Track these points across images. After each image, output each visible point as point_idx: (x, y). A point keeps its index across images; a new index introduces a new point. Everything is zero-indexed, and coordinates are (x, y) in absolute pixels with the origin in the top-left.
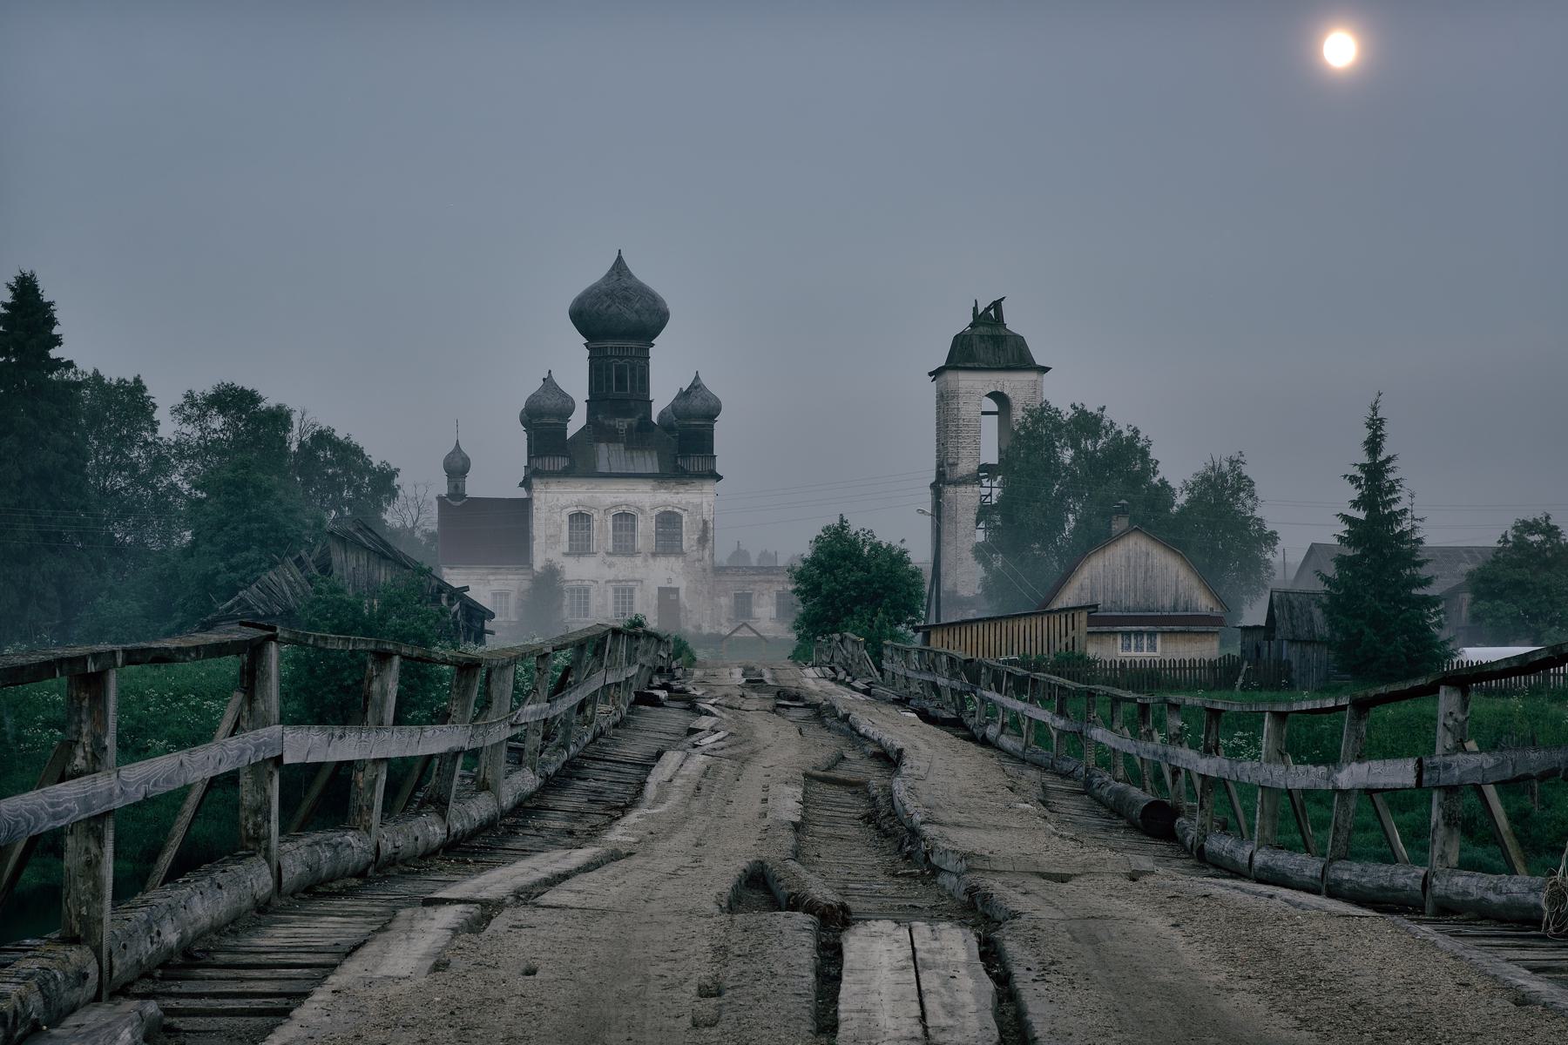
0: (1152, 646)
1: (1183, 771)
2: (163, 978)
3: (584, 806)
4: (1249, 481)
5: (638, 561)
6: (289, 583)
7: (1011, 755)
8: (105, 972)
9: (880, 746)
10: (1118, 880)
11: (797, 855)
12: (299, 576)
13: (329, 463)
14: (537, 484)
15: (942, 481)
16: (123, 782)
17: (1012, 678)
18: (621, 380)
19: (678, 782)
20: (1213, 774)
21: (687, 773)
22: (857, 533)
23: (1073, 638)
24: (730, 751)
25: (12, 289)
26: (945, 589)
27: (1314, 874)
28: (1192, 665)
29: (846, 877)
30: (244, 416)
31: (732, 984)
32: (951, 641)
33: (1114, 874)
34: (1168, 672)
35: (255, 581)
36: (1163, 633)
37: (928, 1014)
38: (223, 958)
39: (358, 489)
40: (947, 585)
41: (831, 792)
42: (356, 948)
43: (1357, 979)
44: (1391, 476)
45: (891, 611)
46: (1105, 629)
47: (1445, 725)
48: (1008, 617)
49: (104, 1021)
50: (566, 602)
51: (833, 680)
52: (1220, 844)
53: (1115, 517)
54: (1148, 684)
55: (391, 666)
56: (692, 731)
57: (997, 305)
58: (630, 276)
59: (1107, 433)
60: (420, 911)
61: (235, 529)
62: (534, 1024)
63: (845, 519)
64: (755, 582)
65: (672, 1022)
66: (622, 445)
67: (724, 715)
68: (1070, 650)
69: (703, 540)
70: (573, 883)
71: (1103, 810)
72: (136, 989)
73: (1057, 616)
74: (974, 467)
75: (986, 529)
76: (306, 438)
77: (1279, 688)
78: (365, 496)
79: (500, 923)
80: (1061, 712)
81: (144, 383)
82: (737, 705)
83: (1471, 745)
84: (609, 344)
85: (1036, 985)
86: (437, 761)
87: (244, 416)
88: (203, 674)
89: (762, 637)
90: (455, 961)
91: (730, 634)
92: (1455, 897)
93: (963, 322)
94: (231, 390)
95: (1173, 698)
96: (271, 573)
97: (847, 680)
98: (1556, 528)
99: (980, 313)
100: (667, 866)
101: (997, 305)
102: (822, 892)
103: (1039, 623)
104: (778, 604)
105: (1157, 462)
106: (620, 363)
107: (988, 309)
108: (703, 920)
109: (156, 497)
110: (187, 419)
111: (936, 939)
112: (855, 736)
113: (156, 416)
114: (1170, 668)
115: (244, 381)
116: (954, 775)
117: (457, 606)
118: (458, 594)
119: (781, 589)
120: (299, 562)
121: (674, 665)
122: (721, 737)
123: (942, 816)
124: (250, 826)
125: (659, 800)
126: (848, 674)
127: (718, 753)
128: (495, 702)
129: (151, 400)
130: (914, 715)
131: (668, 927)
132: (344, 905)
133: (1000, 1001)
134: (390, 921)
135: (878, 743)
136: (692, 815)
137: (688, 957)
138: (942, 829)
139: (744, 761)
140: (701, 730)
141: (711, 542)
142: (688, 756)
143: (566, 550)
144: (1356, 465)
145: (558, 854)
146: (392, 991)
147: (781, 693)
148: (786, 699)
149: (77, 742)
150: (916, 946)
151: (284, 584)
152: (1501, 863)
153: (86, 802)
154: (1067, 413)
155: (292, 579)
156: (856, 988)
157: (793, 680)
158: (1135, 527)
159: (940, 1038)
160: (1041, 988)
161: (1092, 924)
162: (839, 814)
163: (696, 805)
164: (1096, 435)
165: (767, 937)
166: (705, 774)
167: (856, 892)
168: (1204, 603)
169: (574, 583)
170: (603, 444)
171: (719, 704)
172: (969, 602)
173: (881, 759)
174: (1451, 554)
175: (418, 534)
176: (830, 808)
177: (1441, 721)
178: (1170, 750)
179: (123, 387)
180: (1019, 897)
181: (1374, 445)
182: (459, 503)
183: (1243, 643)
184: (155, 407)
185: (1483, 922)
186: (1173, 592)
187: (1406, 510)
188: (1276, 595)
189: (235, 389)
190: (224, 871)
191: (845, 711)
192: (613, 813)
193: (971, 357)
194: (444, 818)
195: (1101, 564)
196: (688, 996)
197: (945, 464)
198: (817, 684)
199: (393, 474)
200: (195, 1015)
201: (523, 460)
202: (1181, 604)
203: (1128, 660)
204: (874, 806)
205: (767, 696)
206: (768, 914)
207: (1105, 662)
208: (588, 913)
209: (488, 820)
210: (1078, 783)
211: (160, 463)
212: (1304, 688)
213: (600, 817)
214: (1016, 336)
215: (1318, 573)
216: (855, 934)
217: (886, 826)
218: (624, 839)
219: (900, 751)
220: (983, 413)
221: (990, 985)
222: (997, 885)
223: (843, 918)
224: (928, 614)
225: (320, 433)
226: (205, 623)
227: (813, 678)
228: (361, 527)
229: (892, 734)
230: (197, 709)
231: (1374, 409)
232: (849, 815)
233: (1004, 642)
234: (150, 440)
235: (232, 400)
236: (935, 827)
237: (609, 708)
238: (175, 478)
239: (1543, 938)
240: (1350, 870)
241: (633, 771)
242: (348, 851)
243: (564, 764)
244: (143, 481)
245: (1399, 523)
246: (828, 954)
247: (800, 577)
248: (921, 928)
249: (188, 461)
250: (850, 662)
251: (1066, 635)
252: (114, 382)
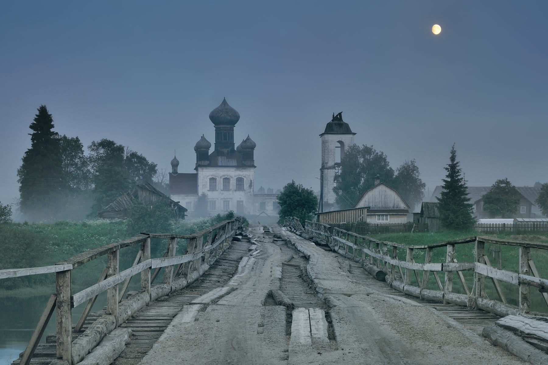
0: (386, 219)
1: (388, 263)
2: (128, 323)
3: (221, 274)
4: (417, 168)
5: (231, 192)
6: (125, 200)
7: (342, 255)
8: (117, 321)
9: (304, 254)
10: (364, 295)
11: (281, 288)
12: (128, 199)
13: (135, 163)
14: (199, 169)
15: (323, 168)
16: (121, 276)
17: (342, 233)
19: (247, 266)
20: (394, 264)
21: (249, 264)
22: (297, 185)
23: (363, 217)
24: (261, 257)
25: (39, 111)
26: (324, 201)
27: (418, 293)
28: (399, 225)
29: (294, 294)
30: (110, 149)
31: (266, 324)
32: (326, 218)
33: (363, 294)
34: (391, 227)
35: (115, 200)
36: (390, 215)
37: (312, 331)
38: (141, 318)
39: (144, 171)
40: (325, 200)
41: (289, 268)
42: (176, 315)
43: (413, 322)
44: (458, 168)
45: (308, 209)
46: (372, 214)
47: (448, 255)
48: (343, 211)
49: (121, 333)
50: (209, 205)
51: (290, 231)
52: (396, 283)
53: (375, 180)
54: (385, 231)
55: (175, 241)
56: (250, 250)
57: (340, 114)
58: (228, 105)
59: (373, 153)
60: (189, 306)
61: (108, 184)
62: (221, 333)
63: (294, 181)
64: (266, 199)
65: (253, 333)
66: (225, 157)
67: (259, 244)
68: (362, 220)
69: (250, 186)
70: (226, 298)
71: (366, 273)
72: (123, 325)
73: (358, 210)
74: (333, 164)
75: (337, 182)
76: (129, 155)
77: (424, 232)
78: (147, 173)
79: (209, 309)
80: (356, 244)
81: (79, 139)
82: (262, 241)
83: (455, 260)
84: (221, 126)
85: (338, 324)
86: (184, 264)
87: (110, 149)
88: (100, 229)
89: (269, 216)
90: (200, 318)
91: (259, 215)
92: (450, 300)
93: (330, 119)
94: (106, 141)
95: (385, 242)
96: (120, 198)
97: (294, 231)
98: (509, 182)
99: (335, 116)
100: (247, 292)
101: (340, 114)
102: (287, 301)
103: (352, 212)
104: (274, 205)
105: (389, 162)
106: (225, 132)
107: (337, 115)
108: (258, 308)
109: (83, 174)
110: (93, 150)
111: (315, 312)
112: (297, 251)
113: (83, 149)
114: (392, 226)
115: (110, 138)
116: (324, 264)
117: (176, 208)
118: (177, 204)
119: (274, 201)
120: (128, 194)
121: (242, 226)
122: (258, 252)
123: (320, 276)
124: (144, 284)
125: (242, 272)
126: (295, 229)
127: (258, 257)
128: (198, 246)
129: (82, 144)
130: (314, 244)
131: (250, 310)
132: (167, 304)
133: (329, 327)
134: (182, 309)
135: (303, 253)
136: (252, 276)
137: (255, 317)
138: (320, 280)
139: (265, 259)
140: (253, 250)
141: (253, 187)
142: (250, 258)
143: (209, 189)
144: (447, 164)
145: (218, 289)
146: (187, 326)
147: (275, 236)
148: (277, 238)
149: (110, 267)
150: (310, 314)
151: (124, 201)
152: (462, 290)
153: (114, 282)
154: (362, 147)
155: (126, 200)
156: (296, 324)
157: (278, 231)
158: (382, 183)
159: (314, 336)
160: (339, 324)
161: (353, 308)
162: (291, 275)
163: (252, 273)
164: (370, 154)
165: (274, 312)
166: (254, 264)
167: (296, 299)
168: (402, 206)
169: (211, 199)
170: (219, 157)
171: (257, 241)
172: (332, 205)
173: (304, 258)
174: (478, 189)
175: (163, 184)
176: (289, 273)
177: (447, 253)
178: (384, 256)
179: (73, 140)
180: (337, 301)
181: (453, 159)
182: (176, 175)
183: (414, 218)
184: (83, 146)
185: (456, 306)
186: (393, 202)
187: (462, 178)
188: (424, 204)
189: (107, 141)
190: (139, 296)
191: (294, 243)
192: (230, 275)
194: (186, 279)
195: (371, 194)
196: (256, 327)
197: (324, 163)
198: (285, 233)
199: (155, 166)
200: (138, 332)
201: (195, 161)
202: (396, 206)
203: (379, 223)
204: (302, 273)
205: (271, 237)
206: (274, 306)
207: (372, 224)
208: (230, 306)
209: (197, 278)
210: (360, 264)
211: (84, 164)
212: (432, 232)
213: (226, 277)
215: (436, 197)
216: (295, 311)
217: (305, 279)
218: (234, 284)
219: (309, 256)
220: (336, 147)
221: (327, 324)
222: (332, 298)
223: (292, 307)
224: (319, 209)
225: (133, 153)
226: (100, 213)
227: (284, 231)
228: (147, 183)
229: (307, 250)
230: (98, 240)
231: (453, 148)
232: (294, 275)
233: (342, 218)
234: (81, 156)
235: (107, 144)
236: (318, 280)
237: (226, 244)
238: (89, 168)
239: (467, 310)
240: (427, 292)
241: (234, 263)
242: (165, 289)
243: (215, 261)
244: (79, 169)
245: (460, 182)
246: (289, 316)
247: (280, 199)
248: (311, 310)
249: (93, 163)
250: (295, 225)
251: (361, 216)
252: (70, 139)
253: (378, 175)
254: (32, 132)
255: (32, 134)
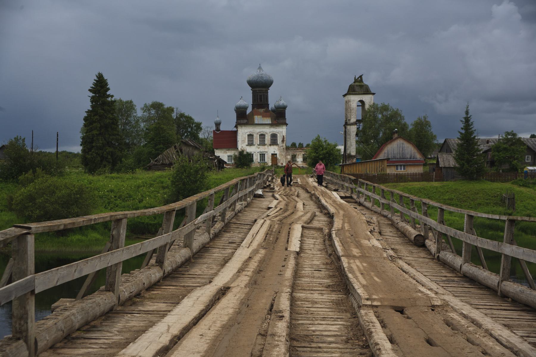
5: (266, 147)
15: (346, 124)
18: (261, 99)
39: (192, 128)
57: (361, 77)
69: (283, 141)
93: (352, 81)
101: (361, 77)
106: (261, 94)
107: (358, 78)
140: (271, 208)
182: (218, 132)
193: (354, 91)
195: (390, 146)
199: (200, 124)
202: (412, 157)
214: (366, 85)
253: (396, 129)
254: (91, 94)
255: (91, 96)
